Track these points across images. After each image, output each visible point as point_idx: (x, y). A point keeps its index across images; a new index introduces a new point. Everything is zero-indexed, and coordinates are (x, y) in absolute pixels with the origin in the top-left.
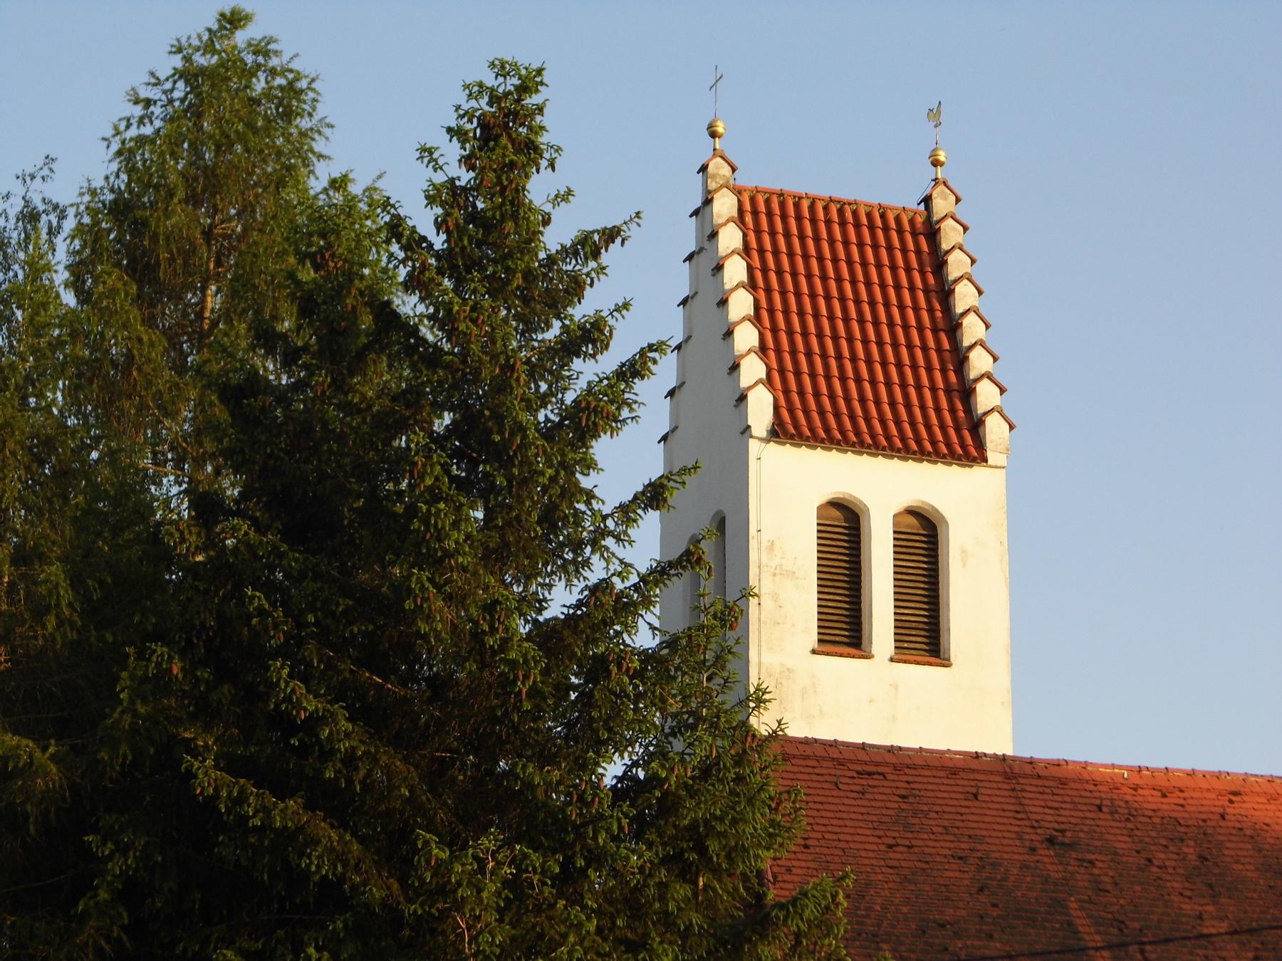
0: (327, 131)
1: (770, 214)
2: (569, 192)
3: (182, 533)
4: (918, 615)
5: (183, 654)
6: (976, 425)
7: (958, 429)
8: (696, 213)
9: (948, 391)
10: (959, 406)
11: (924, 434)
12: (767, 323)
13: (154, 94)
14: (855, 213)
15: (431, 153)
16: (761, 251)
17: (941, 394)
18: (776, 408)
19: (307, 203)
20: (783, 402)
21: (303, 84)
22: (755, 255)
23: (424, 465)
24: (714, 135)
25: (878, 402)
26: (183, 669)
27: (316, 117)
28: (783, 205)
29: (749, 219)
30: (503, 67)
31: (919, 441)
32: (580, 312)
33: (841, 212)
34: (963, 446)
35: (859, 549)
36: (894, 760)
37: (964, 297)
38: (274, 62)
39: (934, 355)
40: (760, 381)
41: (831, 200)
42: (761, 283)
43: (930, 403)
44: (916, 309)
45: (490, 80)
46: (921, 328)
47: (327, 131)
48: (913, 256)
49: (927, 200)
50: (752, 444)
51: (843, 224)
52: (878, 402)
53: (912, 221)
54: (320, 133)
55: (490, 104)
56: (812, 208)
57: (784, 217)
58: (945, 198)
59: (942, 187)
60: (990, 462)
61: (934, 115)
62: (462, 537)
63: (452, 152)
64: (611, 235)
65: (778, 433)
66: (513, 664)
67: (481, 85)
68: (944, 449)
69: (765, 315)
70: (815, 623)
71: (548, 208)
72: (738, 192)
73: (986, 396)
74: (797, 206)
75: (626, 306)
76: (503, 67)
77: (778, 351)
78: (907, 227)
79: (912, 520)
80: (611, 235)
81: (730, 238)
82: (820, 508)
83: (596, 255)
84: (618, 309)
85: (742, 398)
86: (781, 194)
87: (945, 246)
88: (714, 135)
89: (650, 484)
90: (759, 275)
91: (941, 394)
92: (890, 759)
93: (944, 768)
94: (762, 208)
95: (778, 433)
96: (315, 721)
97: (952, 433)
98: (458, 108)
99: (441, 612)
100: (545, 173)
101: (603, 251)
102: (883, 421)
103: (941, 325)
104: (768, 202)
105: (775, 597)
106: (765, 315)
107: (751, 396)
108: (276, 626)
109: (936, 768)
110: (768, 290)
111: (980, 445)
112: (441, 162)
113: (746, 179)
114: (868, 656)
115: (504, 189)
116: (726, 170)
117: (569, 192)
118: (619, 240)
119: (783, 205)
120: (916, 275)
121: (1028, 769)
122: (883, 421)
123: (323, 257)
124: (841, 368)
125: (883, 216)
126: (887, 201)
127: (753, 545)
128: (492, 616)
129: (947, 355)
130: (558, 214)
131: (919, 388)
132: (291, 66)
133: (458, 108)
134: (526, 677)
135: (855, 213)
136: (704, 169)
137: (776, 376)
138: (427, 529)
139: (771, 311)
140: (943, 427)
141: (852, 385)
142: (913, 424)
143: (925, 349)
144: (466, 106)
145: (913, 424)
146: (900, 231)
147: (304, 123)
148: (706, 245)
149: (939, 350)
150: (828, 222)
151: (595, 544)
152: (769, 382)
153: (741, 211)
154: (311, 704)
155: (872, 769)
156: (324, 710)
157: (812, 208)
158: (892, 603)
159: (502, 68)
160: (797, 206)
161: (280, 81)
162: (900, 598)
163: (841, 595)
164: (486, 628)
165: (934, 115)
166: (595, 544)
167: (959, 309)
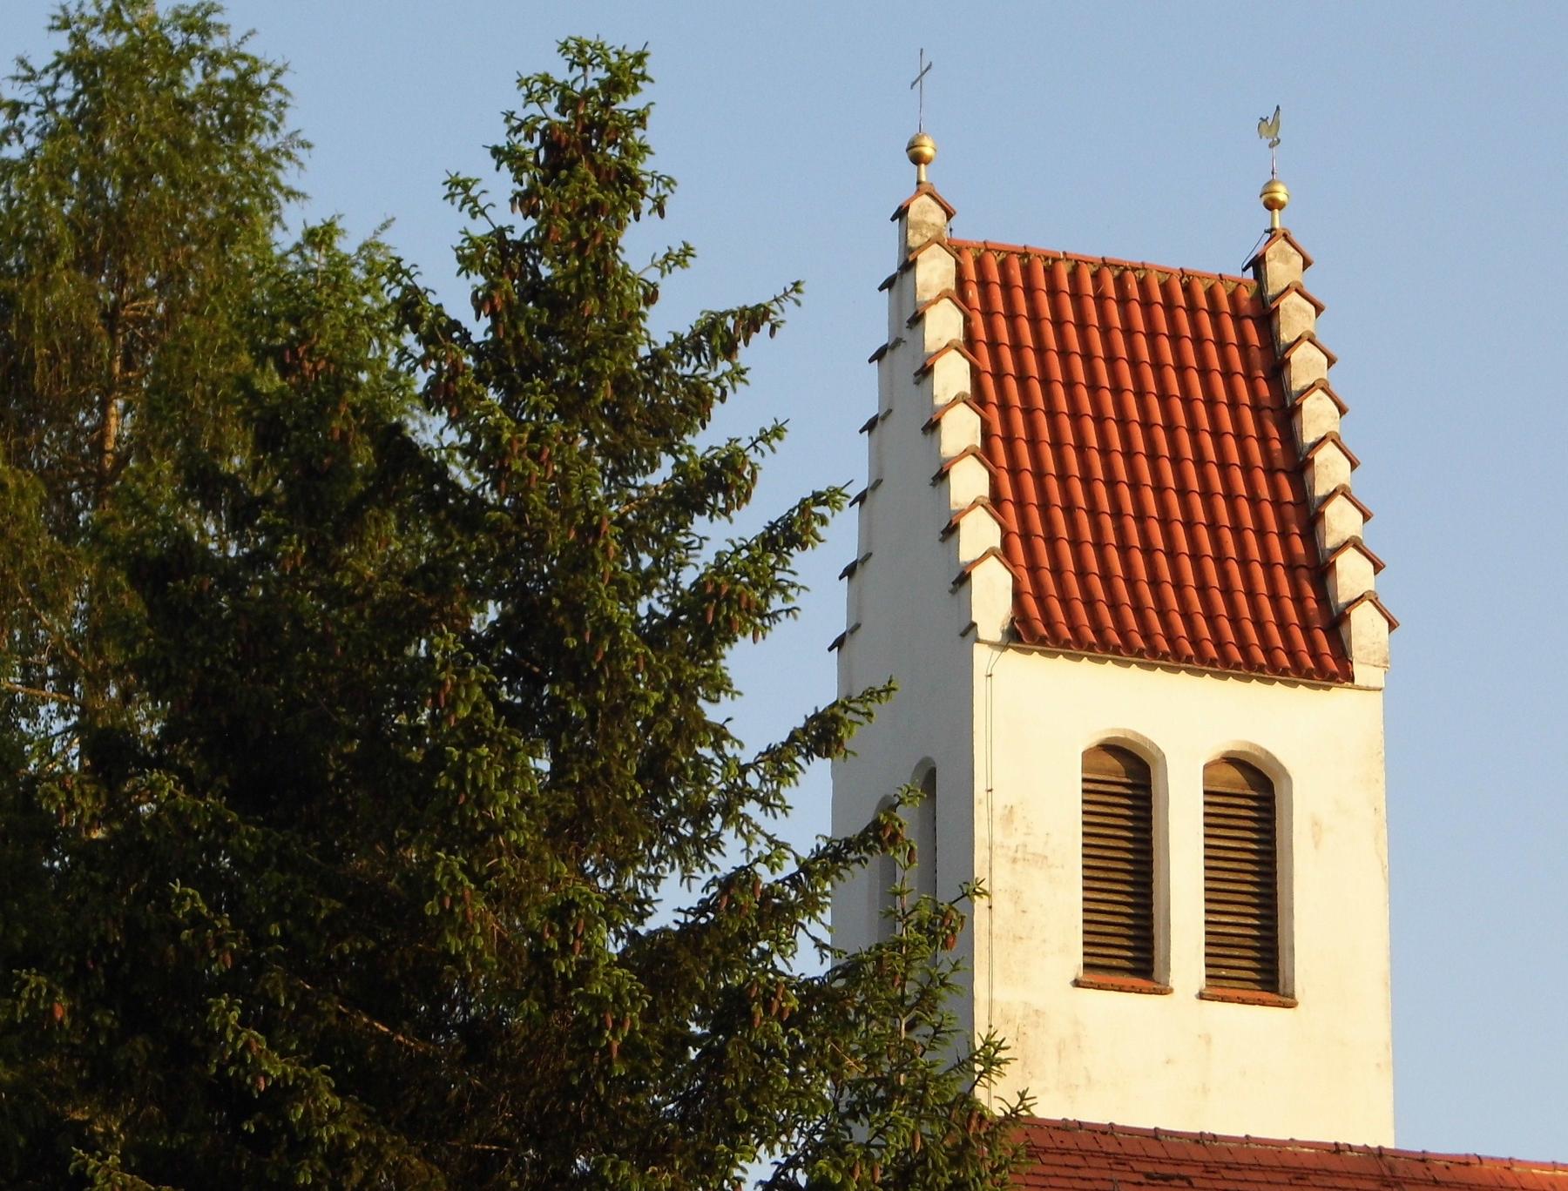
0: (301, 153)
1: (1007, 286)
2: (687, 251)
3: (69, 794)
4: (1244, 925)
5: (71, 987)
6: (1336, 622)
7: (1307, 629)
8: (889, 284)
9: (1291, 567)
10: (1309, 591)
11: (1253, 637)
12: (1002, 459)
13: (25, 94)
14: (1143, 285)
15: (466, 189)
16: (994, 345)
17: (1280, 573)
18: (1017, 595)
19: (270, 267)
20: (1027, 585)
21: (263, 78)
22: (983, 350)
23: (456, 686)
24: (917, 159)
25: (1179, 586)
26: (71, 1011)
27: (284, 131)
28: (1027, 271)
29: (973, 293)
30: (581, 51)
31: (1244, 648)
32: (704, 441)
33: (1120, 282)
34: (1315, 655)
35: (1149, 820)
36: (1205, 1156)
37: (1316, 417)
38: (217, 43)
39: (1268, 511)
40: (991, 552)
41: (1105, 263)
42: (992, 395)
43: (1262, 587)
44: (1240, 437)
45: (561, 72)
46: (1247, 468)
47: (301, 153)
48: (1234, 353)
49: (1258, 264)
50: (981, 654)
51: (1123, 301)
52: (1179, 586)
53: (1233, 298)
54: (289, 156)
55: (561, 109)
56: (1074, 275)
57: (1030, 290)
58: (1287, 261)
59: (926, 199)
60: (1357, 682)
61: (1269, 127)
62: (516, 801)
63: (499, 186)
64: (754, 319)
65: (1020, 634)
66: (597, 1003)
67: (546, 80)
68: (1284, 661)
69: (999, 446)
70: (1079, 938)
71: (653, 276)
72: (956, 250)
73: (1351, 575)
74: (1050, 272)
75: (778, 432)
76: (581, 51)
77: (1021, 504)
78: (1225, 306)
79: (1234, 774)
80: (754, 319)
81: (944, 324)
82: (1086, 755)
83: (729, 350)
84: (765, 436)
85: (963, 579)
86: (1025, 254)
87: (1286, 336)
88: (917, 159)
89: (817, 716)
90: (989, 382)
91: (1280, 573)
92: (1199, 1154)
93: (1284, 1169)
94: (995, 275)
95: (1020, 634)
96: (282, 1094)
97: (1298, 635)
98: (509, 116)
99: (482, 919)
100: (649, 220)
101: (741, 344)
102: (1187, 617)
103: (1280, 462)
104: (1004, 266)
105: (1016, 896)
106: (999, 446)
107: (977, 574)
108: (219, 942)
109: (1272, 1169)
110: (1005, 407)
111: (1342, 654)
112: (482, 202)
113: (968, 230)
114: (1164, 991)
115: (582, 245)
116: (936, 216)
117: (687, 251)
118: (765, 328)
119: (1027, 271)
120: (1241, 384)
121: (1419, 1171)
122: (1187, 617)
123: (294, 353)
124: (1121, 531)
125: (1187, 289)
126: (1190, 267)
127: (980, 812)
128: (564, 926)
129: (1290, 511)
130: (671, 286)
131: (1244, 562)
132: (244, 49)
133: (509, 116)
134: (618, 1023)
135: (1143, 285)
136: (901, 213)
137: (1017, 543)
138: (461, 788)
139: (1009, 440)
140: (1283, 625)
141: (1138, 558)
142: (1235, 620)
143: (1254, 500)
144: (522, 114)
145: (1235, 620)
146: (1215, 313)
147: (265, 141)
148: (906, 334)
149: (1277, 503)
150: (1100, 298)
151: (728, 811)
152: (1005, 554)
153: (961, 280)
154: (276, 1068)
155: (1168, 1170)
156: (297, 1076)
157: (1074, 275)
158: (1202, 906)
159: (580, 53)
160: (1050, 272)
161: (225, 73)
162: (1214, 898)
163: (1119, 895)
164: (555, 945)
165: (1269, 127)
166: (728, 811)
167: (1309, 437)
